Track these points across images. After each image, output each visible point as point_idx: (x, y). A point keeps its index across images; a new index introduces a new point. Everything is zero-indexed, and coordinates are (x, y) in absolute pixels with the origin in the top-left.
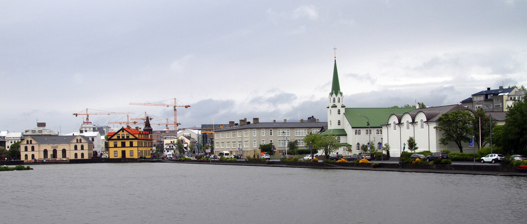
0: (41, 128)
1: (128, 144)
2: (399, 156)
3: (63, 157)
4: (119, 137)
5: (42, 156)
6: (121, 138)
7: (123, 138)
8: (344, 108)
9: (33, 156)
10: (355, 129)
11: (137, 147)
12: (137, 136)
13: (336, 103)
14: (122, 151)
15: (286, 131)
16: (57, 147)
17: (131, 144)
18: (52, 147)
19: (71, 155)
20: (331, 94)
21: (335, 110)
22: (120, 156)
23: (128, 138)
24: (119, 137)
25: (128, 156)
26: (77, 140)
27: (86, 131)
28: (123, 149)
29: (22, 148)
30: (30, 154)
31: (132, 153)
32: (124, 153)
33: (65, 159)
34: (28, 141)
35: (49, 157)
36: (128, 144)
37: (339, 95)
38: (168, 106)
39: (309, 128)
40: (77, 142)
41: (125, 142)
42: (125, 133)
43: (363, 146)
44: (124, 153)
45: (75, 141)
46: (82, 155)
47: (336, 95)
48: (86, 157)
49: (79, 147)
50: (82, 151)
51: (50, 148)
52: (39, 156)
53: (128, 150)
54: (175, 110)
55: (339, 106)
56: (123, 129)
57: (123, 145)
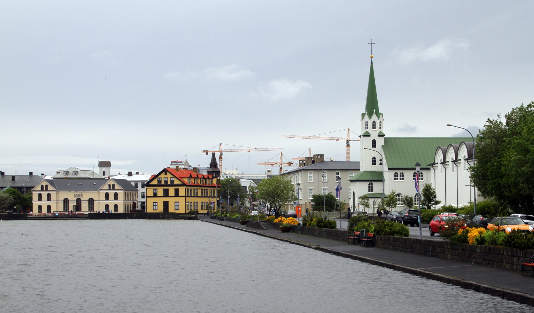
0: (104, 169)
1: (172, 192)
2: (162, 212)
3: (64, 210)
4: (160, 182)
5: (61, 208)
6: (163, 183)
7: (166, 184)
8: (382, 138)
9: (49, 207)
10: (393, 172)
11: (185, 196)
12: (186, 180)
13: (370, 130)
14: (164, 202)
15: (327, 174)
16: (82, 195)
17: (177, 191)
18: (75, 196)
19: (99, 207)
20: (363, 115)
21: (368, 141)
22: (160, 209)
23: (172, 184)
24: (161, 181)
25: (171, 209)
26: (109, 185)
27: (137, 173)
28: (166, 199)
29: (35, 197)
30: (44, 204)
31: (177, 204)
32: (166, 204)
33: (67, 213)
34: (42, 187)
35: (71, 209)
36: (172, 192)
37: (374, 117)
38: (338, 140)
39: (317, 170)
40: (109, 189)
41: (167, 190)
42: (169, 176)
43: (406, 198)
44: (166, 204)
45: (106, 187)
46: (116, 207)
47: (370, 116)
48: (121, 210)
49: (111, 196)
50: (116, 202)
51: (72, 197)
52: (57, 207)
53: (172, 201)
54: (348, 145)
55: (374, 134)
56: (165, 171)
57: (166, 194)
